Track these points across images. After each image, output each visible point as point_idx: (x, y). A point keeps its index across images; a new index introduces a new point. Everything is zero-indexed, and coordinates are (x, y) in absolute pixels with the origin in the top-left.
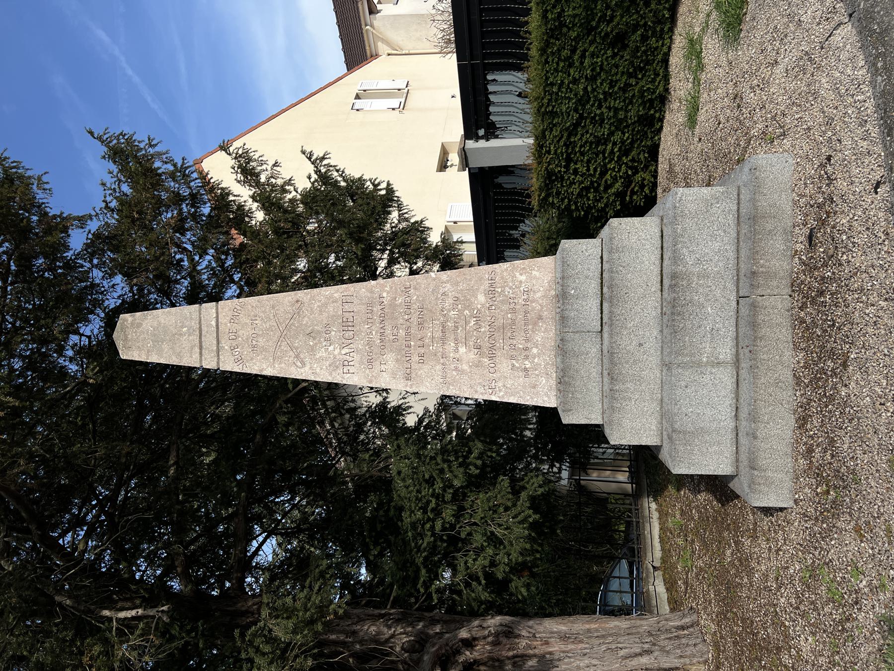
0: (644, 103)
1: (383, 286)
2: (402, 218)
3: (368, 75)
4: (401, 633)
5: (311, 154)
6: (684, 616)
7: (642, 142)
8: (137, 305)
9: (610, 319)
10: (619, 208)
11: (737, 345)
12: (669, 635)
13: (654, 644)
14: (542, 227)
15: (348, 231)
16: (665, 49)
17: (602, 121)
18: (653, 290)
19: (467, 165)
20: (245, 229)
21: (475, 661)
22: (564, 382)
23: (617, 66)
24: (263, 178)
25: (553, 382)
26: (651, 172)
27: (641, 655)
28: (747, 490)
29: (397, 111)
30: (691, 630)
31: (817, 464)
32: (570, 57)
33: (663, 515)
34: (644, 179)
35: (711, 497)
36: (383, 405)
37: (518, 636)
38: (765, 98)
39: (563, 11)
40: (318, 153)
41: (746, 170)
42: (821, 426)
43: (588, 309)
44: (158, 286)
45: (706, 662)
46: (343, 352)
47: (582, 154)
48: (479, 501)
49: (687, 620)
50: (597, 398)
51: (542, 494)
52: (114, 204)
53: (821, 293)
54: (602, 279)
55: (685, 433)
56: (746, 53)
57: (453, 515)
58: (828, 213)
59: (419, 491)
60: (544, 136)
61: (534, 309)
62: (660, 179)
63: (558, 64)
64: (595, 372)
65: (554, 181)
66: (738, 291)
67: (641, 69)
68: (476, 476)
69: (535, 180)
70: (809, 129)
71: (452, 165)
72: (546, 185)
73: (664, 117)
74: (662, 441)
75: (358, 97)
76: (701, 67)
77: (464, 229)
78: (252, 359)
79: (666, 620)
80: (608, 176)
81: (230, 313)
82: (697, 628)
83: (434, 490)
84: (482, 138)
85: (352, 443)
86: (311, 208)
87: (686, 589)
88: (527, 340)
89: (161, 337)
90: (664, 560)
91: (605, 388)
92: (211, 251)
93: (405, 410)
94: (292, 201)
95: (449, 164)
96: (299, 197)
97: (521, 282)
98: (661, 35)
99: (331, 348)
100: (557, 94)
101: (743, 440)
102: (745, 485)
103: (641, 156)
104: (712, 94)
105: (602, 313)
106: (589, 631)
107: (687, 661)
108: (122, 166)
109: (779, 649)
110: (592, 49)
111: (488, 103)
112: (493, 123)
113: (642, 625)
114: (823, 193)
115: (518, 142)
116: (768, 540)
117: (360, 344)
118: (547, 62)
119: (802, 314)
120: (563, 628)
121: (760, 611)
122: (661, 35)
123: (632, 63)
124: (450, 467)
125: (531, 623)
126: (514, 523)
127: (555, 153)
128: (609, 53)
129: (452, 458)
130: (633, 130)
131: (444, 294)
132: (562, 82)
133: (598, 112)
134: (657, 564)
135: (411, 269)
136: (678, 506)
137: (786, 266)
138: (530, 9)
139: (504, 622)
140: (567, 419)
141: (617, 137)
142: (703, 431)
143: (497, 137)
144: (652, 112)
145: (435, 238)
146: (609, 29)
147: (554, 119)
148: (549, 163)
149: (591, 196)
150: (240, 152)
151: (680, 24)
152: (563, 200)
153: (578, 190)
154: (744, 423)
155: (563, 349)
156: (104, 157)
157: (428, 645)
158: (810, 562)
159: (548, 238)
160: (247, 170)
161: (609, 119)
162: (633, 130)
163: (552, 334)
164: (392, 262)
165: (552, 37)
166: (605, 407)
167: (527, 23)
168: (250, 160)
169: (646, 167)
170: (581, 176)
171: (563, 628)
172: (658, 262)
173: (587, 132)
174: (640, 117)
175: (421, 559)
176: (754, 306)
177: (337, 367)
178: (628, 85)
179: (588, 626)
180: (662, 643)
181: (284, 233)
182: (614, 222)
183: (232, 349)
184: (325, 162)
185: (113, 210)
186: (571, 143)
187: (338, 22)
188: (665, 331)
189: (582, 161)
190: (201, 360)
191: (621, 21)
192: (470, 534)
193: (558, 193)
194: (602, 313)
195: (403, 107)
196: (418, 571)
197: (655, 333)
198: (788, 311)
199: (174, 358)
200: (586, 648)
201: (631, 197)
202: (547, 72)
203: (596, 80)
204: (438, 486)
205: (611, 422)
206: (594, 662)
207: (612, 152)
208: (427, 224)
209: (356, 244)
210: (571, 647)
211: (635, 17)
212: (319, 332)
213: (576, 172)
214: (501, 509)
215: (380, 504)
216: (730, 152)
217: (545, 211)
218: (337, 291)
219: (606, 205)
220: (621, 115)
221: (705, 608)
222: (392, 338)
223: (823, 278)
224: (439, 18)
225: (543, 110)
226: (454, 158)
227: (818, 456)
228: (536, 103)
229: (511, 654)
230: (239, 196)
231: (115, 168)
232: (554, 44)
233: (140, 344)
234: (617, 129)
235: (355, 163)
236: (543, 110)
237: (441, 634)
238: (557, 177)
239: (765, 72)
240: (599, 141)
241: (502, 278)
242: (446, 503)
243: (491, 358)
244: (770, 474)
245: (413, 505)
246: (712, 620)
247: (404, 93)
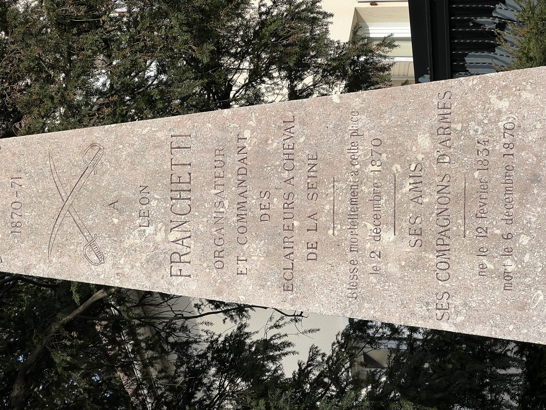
14: (537, 11)
36: (237, 341)
46: (175, 235)
78: (11, 248)
88: (510, 221)
97: (499, 112)
99: (150, 230)
117: (200, 224)
135: (292, 88)
145: (339, 32)
164: (256, 75)
177: (160, 264)
181: (73, 24)
212: (129, 201)
241: (464, 104)
243: (441, 253)
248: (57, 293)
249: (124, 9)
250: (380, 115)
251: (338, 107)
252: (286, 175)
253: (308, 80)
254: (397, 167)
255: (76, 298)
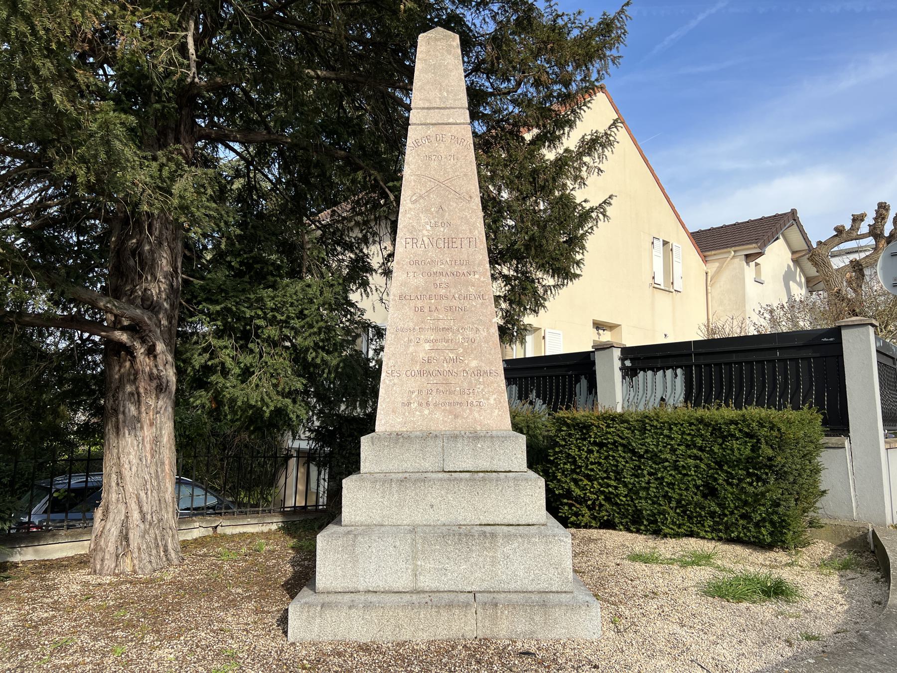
0: (654, 515)
1: (484, 274)
2: (546, 288)
3: (686, 254)
4: (159, 288)
5: (610, 204)
6: (177, 552)
7: (618, 513)
8: (467, 44)
9: (456, 479)
10: (557, 492)
11: (431, 592)
12: (159, 538)
13: (150, 524)
14: (539, 420)
15: (535, 237)
16: (702, 534)
17: (637, 476)
18: (481, 517)
19: (597, 350)
20: (538, 141)
21: (135, 357)
22: (398, 438)
23: (687, 489)
24: (586, 159)
25: (398, 428)
26: (590, 522)
27: (141, 512)
28: (303, 601)
29: (651, 281)
30: (164, 559)
31: (328, 660)
32: (695, 446)
33: (267, 535)
34: (583, 516)
35: (289, 575)
36: (369, 269)
37: (158, 398)
38: (652, 617)
39: (737, 439)
40: (609, 210)
41: (588, 598)
42: (361, 663)
43: (464, 459)
44: (487, 61)
45: (135, 572)
46: (426, 240)
47: (606, 458)
48: (282, 362)
49: (173, 555)
50: (384, 468)
51: (290, 419)
52: (560, 22)
53: (478, 662)
54: (491, 472)
55: (354, 545)
56: (693, 602)
57: (269, 337)
58: (549, 667)
59: (292, 305)
60: (623, 422)
61: (464, 411)
62: (583, 531)
63: (689, 434)
64: (408, 466)
65: (581, 431)
66: (480, 592)
67: (684, 512)
68: (305, 359)
69: (583, 413)
70: (623, 651)
71: (599, 334)
72: (578, 424)
73: (641, 534)
74: (346, 526)
75: (665, 243)
76: (684, 565)
77: (537, 346)
78: (418, 155)
79: (173, 536)
80: (586, 482)
81: (460, 136)
82: (166, 564)
83: (293, 319)
84: (623, 364)
85: (334, 237)
86: (557, 203)
87: (200, 556)
88: (436, 405)
89: (438, 70)
90: (224, 536)
91: (393, 475)
92: (516, 111)
93: (365, 291)
94: (564, 186)
95: (601, 331)
96: (568, 192)
97: (488, 399)
98: (716, 530)
99: (428, 227)
100: (662, 434)
101: (347, 597)
102: (307, 600)
103: (604, 513)
104: (659, 575)
105: (460, 472)
106: (163, 463)
107: (136, 555)
108: (596, 31)
109: (158, 632)
110: (702, 466)
111: (655, 370)
112: (636, 374)
113: (168, 513)
114: (566, 663)
115: (619, 397)
116: (256, 623)
117: (432, 253)
118: (691, 424)
119: (460, 647)
120: (165, 439)
121: (190, 617)
122: (716, 530)
123: (690, 503)
124: (314, 333)
125: (170, 409)
126: (262, 393)
127: (607, 433)
128: (699, 482)
129: (322, 336)
130: (629, 505)
131: (477, 330)
132: (672, 439)
133: (645, 472)
134: (219, 530)
135: (499, 296)
136: (278, 548)
137: (503, 633)
138: (741, 409)
139: (170, 383)
140: (365, 440)
141: (622, 490)
142: (355, 561)
143: (624, 378)
144: (645, 523)
145: (528, 319)
146: (720, 481)
147: (639, 431)
148: (598, 427)
149: (568, 466)
150: (611, 138)
151: (726, 547)
152: (564, 440)
153: (573, 454)
154: (363, 598)
155: (428, 437)
156: (605, 14)
157: (150, 313)
158: (240, 655)
159: (528, 426)
160: (594, 144)
161: (638, 482)
162: (629, 505)
163: (442, 427)
164: (507, 279)
165: (714, 429)
166: (375, 475)
167: (727, 405)
168: (603, 146)
169: (595, 518)
170: (586, 457)
171: (165, 439)
172: (506, 521)
173: (627, 462)
174: (641, 511)
175: (230, 305)
176: (467, 605)
177: (411, 233)
178: (670, 499)
179: (167, 462)
180: (152, 531)
181: (534, 179)
182: (542, 482)
183: (428, 138)
184: (601, 216)
185: (555, 21)
186: (617, 447)
187: (739, 224)
188: (444, 528)
189: (600, 458)
190: (417, 108)
191: (728, 493)
192: (252, 351)
193: (570, 435)
194: (460, 472)
195: (656, 287)
196: (217, 302)
197: (443, 520)
198: (463, 636)
199: (419, 84)
200: (146, 460)
201: (566, 504)
202: (682, 425)
203: (675, 470)
204: (296, 323)
205: (363, 480)
206: (134, 469)
207: (608, 486)
208: (542, 311)
209: (523, 245)
210: (148, 447)
211: (732, 505)
212: (443, 216)
213: (590, 452)
214: (275, 381)
215: (279, 268)
216: (605, 589)
217: (554, 424)
218: (480, 234)
219: (559, 481)
220: (643, 494)
221: (185, 571)
222: (438, 283)
223: (492, 663)
224: (735, 323)
225: (647, 421)
226: (606, 337)
227: (336, 660)
228: (653, 414)
229: (142, 390)
230: (568, 136)
231: (594, 24)
232: (707, 432)
233: (432, 53)
234: (630, 490)
235: (598, 247)
236: (647, 421)
237: (159, 324)
238: (585, 434)
239: (675, 617)
240: (618, 473)
241: (492, 382)
242: (281, 329)
243: (420, 372)
244: (318, 620)
245: (279, 299)
246: (175, 577)
247: (669, 288)
248: (395, 177)
249: (542, 208)
250: (487, 342)
251: (490, 321)
252: (457, 296)
253: (504, 305)
254: (461, 350)
255: (390, 184)
